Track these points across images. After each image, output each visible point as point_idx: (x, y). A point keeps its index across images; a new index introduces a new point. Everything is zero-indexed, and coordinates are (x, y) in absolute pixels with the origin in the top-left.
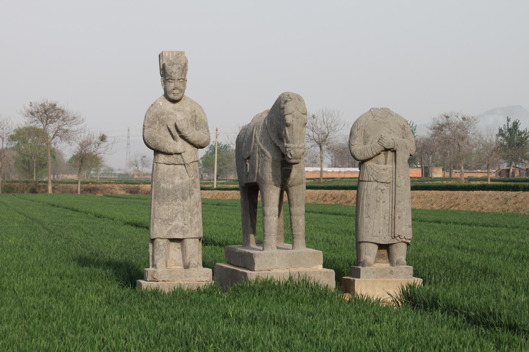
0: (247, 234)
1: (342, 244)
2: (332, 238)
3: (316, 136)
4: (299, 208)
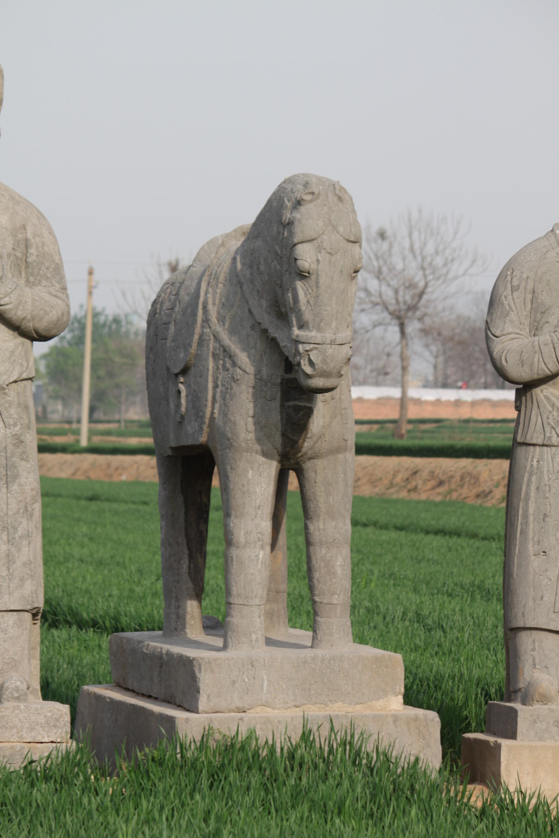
0: (177, 600)
1: (462, 630)
2: (434, 610)
3: (388, 294)
4: (333, 524)
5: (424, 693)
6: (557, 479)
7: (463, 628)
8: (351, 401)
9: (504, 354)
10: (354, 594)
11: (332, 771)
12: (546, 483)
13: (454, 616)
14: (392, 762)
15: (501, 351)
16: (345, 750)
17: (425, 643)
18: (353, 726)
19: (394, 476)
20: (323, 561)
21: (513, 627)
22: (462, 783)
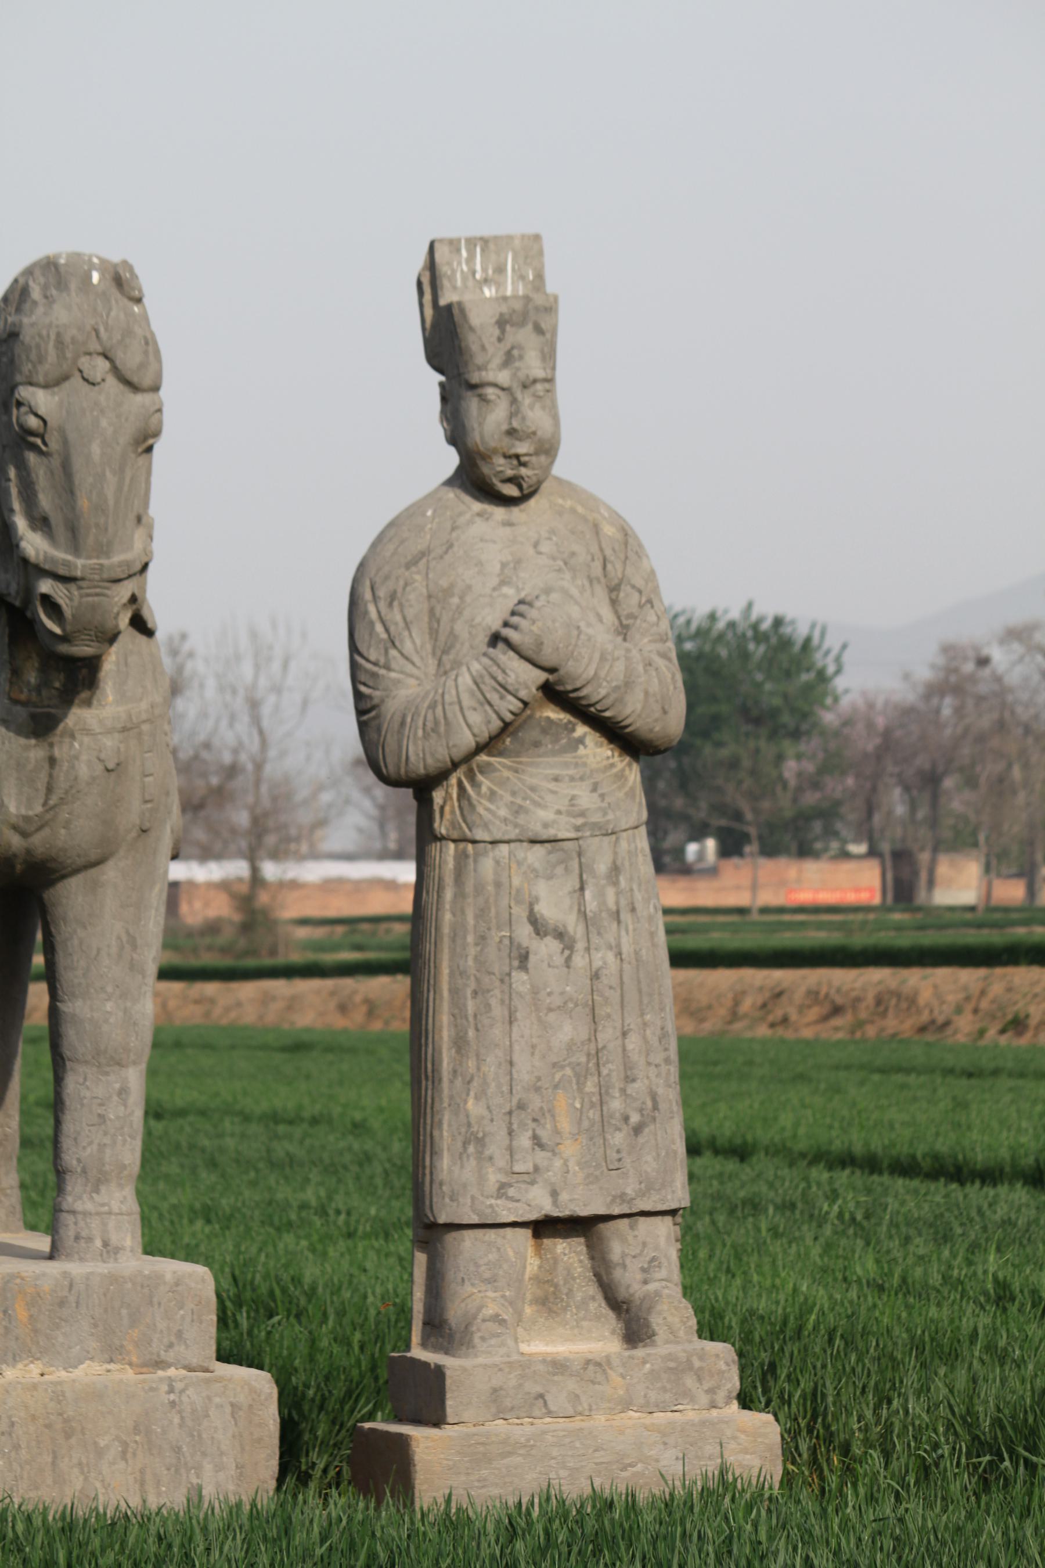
19: (737, 1003)
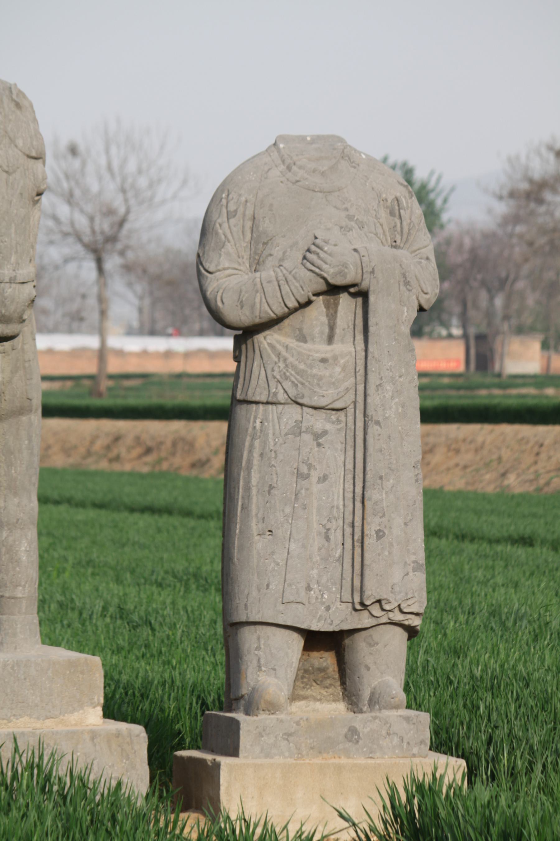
1: (173, 626)
3: (82, 222)
4: (16, 500)
5: (128, 703)
6: (285, 443)
7: (175, 624)
8: (35, 352)
9: (219, 294)
10: (44, 585)
11: (16, 801)
12: (272, 448)
13: (164, 610)
14: (89, 788)
15: (216, 290)
16: (32, 775)
17: (129, 643)
18: (41, 746)
19: (92, 442)
20: (3, 545)
21: (234, 622)
22: (173, 811)
